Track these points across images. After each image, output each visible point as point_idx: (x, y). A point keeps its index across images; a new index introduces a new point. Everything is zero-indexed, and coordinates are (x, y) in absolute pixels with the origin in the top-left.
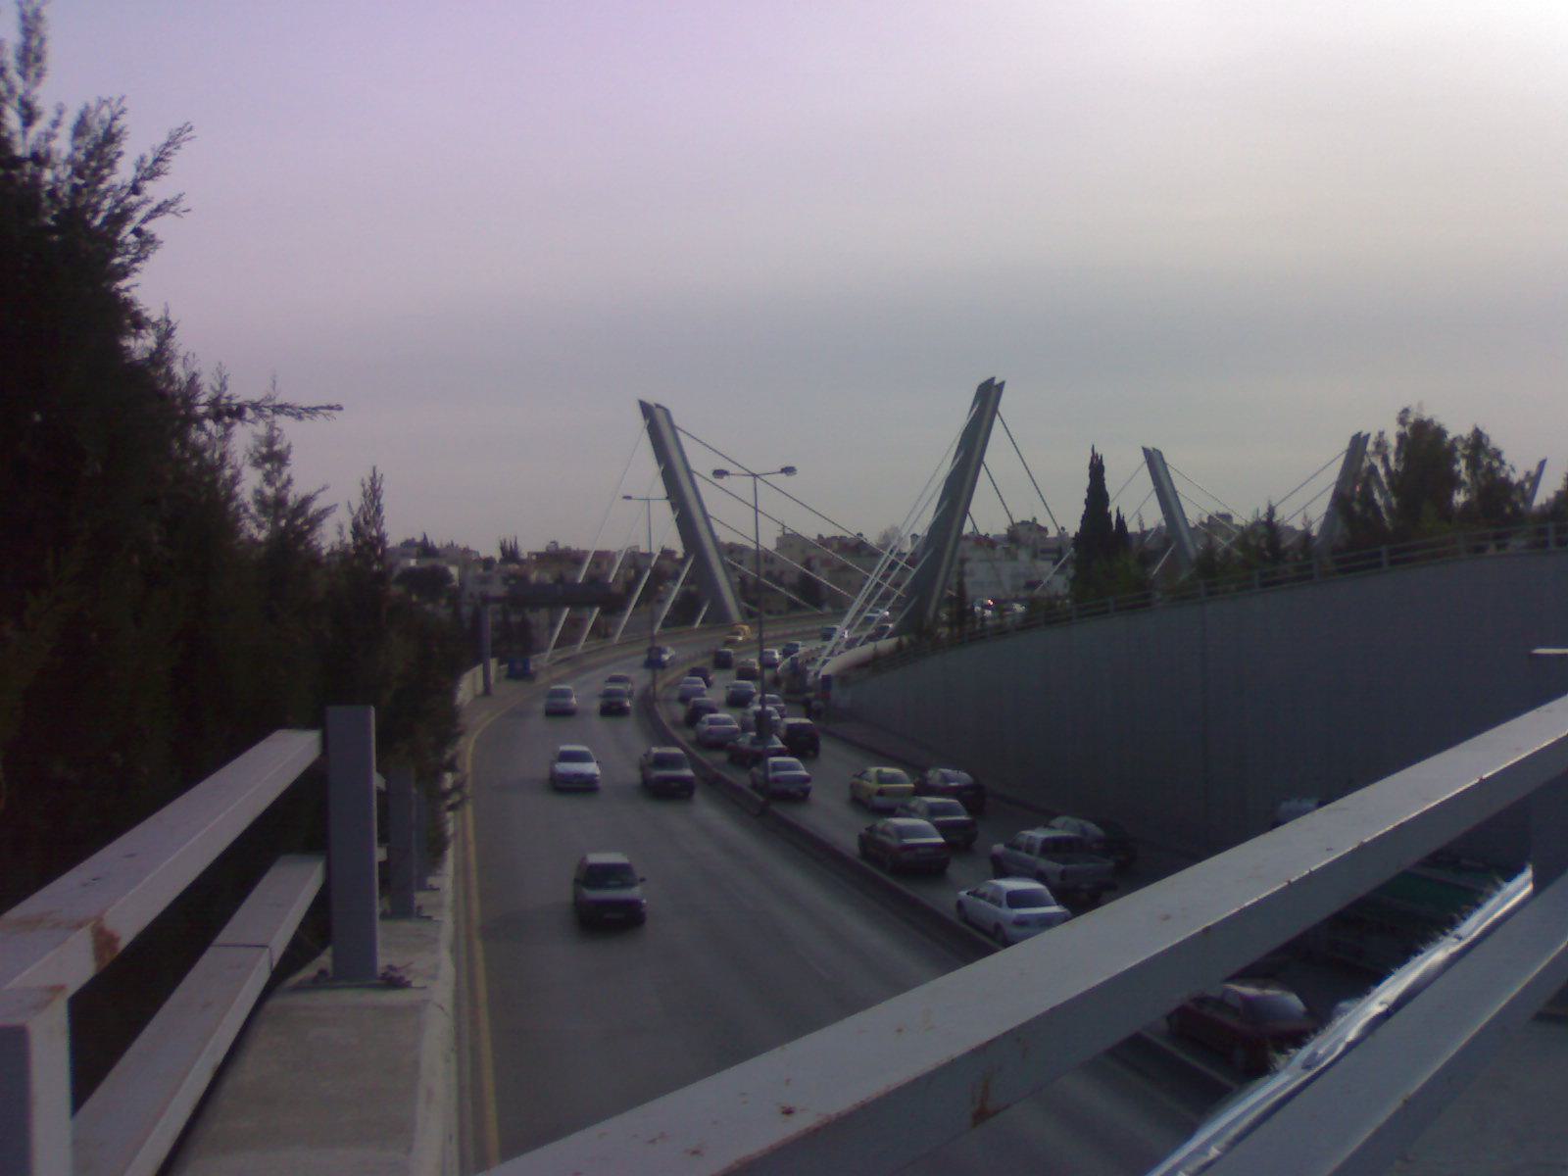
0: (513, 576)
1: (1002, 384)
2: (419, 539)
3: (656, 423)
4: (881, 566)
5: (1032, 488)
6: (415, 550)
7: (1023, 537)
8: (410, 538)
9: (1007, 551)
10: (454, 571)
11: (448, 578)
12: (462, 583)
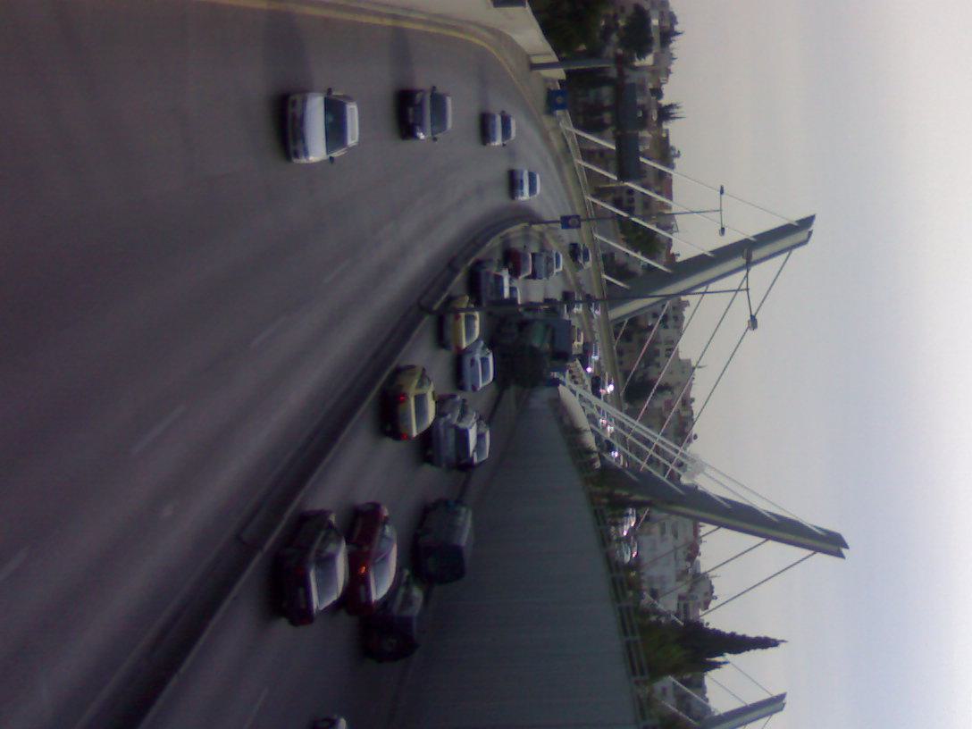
0: (646, 115)
1: (841, 555)
2: (677, 28)
3: (794, 233)
4: (669, 445)
5: (742, 582)
6: (667, 24)
7: (699, 587)
8: (679, 20)
9: (685, 572)
10: (649, 60)
11: (642, 54)
12: (636, 69)
